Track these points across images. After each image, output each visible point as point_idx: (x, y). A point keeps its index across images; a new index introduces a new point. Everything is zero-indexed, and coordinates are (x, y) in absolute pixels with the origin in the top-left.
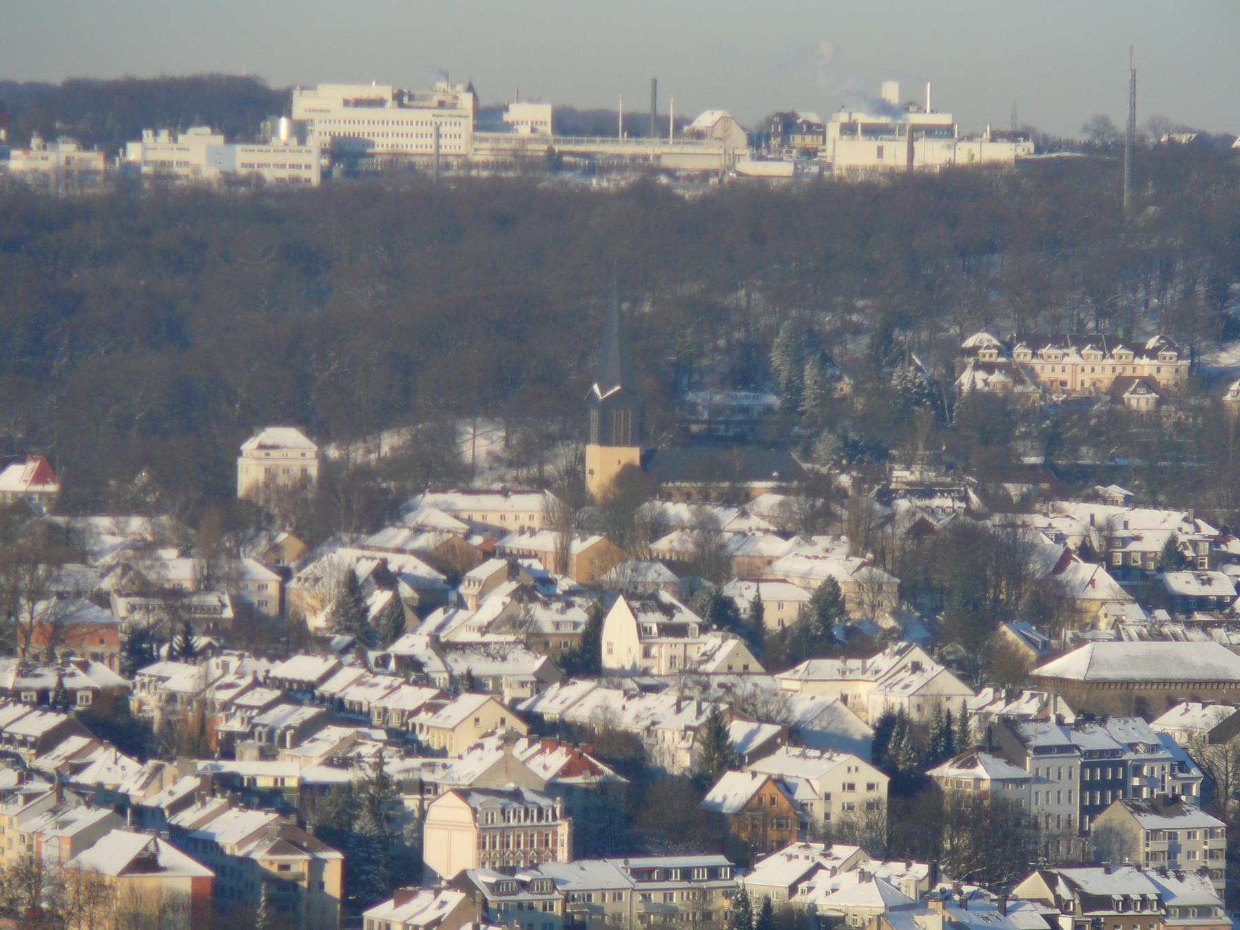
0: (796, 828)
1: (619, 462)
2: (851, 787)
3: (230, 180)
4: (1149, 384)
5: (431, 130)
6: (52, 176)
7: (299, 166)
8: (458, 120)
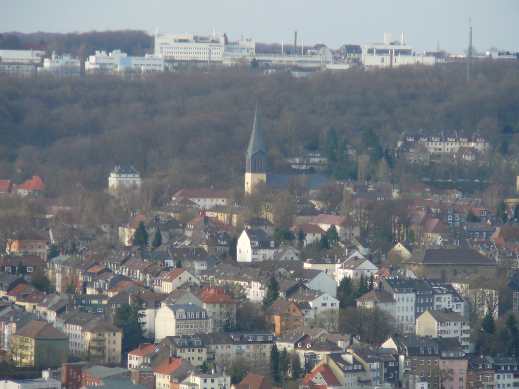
0: (328, 321)
1: (258, 179)
2: (325, 305)
3: (129, 71)
4: (474, 151)
5: (207, 51)
6: (60, 69)
7: (156, 65)
8: (219, 47)
